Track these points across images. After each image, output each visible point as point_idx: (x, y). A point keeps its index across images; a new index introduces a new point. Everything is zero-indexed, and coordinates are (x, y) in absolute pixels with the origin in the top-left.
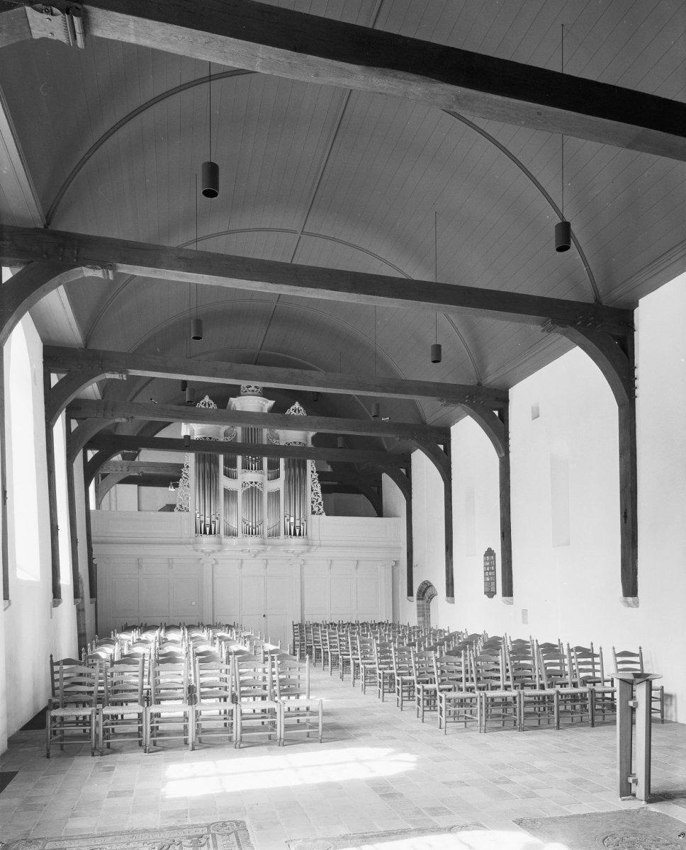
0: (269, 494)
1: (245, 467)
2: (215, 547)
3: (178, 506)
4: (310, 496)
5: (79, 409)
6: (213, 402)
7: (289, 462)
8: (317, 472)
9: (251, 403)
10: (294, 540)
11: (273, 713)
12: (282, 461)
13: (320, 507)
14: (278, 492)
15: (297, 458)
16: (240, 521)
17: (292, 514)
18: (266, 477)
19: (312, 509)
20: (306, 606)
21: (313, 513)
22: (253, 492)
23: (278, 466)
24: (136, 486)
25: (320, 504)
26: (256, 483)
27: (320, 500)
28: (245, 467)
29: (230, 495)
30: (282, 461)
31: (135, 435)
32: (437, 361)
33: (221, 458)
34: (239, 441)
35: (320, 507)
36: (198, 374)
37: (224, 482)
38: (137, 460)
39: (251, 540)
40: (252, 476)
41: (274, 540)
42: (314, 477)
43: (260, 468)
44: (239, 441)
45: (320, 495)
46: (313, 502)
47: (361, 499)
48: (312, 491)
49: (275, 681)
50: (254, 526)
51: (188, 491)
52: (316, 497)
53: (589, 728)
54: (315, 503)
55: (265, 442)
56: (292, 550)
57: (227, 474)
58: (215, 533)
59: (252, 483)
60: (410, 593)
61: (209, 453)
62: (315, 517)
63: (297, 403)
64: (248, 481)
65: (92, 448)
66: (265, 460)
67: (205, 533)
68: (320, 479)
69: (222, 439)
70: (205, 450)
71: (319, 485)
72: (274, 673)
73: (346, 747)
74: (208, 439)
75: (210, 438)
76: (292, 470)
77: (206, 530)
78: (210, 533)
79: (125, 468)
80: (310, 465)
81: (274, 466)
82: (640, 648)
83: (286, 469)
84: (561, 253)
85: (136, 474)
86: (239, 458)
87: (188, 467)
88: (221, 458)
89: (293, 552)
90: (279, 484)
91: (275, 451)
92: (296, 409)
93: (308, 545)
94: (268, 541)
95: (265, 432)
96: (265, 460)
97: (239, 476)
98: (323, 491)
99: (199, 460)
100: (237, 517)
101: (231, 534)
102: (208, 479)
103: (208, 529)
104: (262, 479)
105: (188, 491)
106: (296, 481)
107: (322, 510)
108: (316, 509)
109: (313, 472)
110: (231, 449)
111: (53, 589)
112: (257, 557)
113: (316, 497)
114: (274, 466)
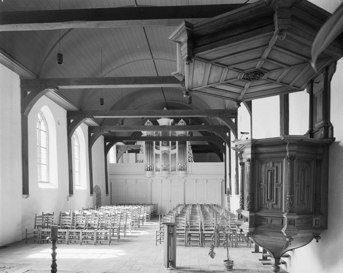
0: (172, 155)
1: (163, 145)
2: (151, 176)
3: (139, 161)
4: (188, 155)
5: (93, 129)
6: (150, 122)
7: (179, 142)
8: (191, 146)
9: (164, 121)
10: (181, 172)
11: (79, 233)
12: (177, 142)
13: (192, 159)
14: (175, 154)
15: (182, 141)
16: (161, 166)
17: (180, 162)
18: (170, 149)
19: (189, 160)
20: (187, 198)
21: (189, 161)
22: (165, 155)
23: (175, 144)
24: (135, 154)
25: (192, 158)
26: (166, 151)
27: (192, 156)
28: (163, 145)
29: (157, 156)
30: (177, 142)
31: (129, 136)
32: (102, 104)
33: (154, 142)
34: (161, 135)
35: (192, 159)
36: (115, 116)
37: (155, 151)
38: (136, 144)
39: (165, 172)
40: (165, 148)
41: (174, 172)
42: (189, 147)
43: (168, 145)
44: (161, 135)
45: (192, 154)
46: (189, 157)
47: (214, 154)
48: (189, 153)
49: (99, 224)
50: (182, 166)
51: (143, 155)
52: (191, 155)
53: (66, 245)
54: (190, 158)
55: (170, 136)
56: (180, 176)
57: (156, 148)
58: (151, 170)
59: (164, 151)
60: (226, 193)
61: (148, 141)
62: (190, 163)
63: (148, 120)
64: (163, 150)
65: (108, 142)
66: (170, 142)
67: (181, 170)
68: (192, 148)
69: (154, 136)
70: (149, 140)
71: (191, 151)
72: (99, 221)
73: (110, 249)
74: (149, 136)
75: (150, 135)
76: (180, 145)
77: (149, 169)
78: (150, 170)
79: (126, 148)
80: (188, 143)
81: (174, 144)
82: (53, 212)
83: (178, 145)
84: (59, 64)
85: (130, 150)
86: (161, 142)
87: (143, 146)
88: (154, 142)
89: (180, 177)
90: (176, 151)
91: (174, 139)
92: (182, 123)
93: (187, 174)
94: (171, 173)
95: (170, 132)
96: (170, 142)
97: (161, 148)
98: (193, 152)
99: (146, 143)
100: (160, 164)
101: (158, 170)
102: (149, 149)
103: (165, 169)
104: (169, 149)
105: (143, 155)
106: (183, 149)
107: (193, 160)
108: (190, 160)
109: (189, 145)
110: (157, 139)
111: (23, 188)
112: (167, 179)
113: (191, 155)
114: (174, 144)
